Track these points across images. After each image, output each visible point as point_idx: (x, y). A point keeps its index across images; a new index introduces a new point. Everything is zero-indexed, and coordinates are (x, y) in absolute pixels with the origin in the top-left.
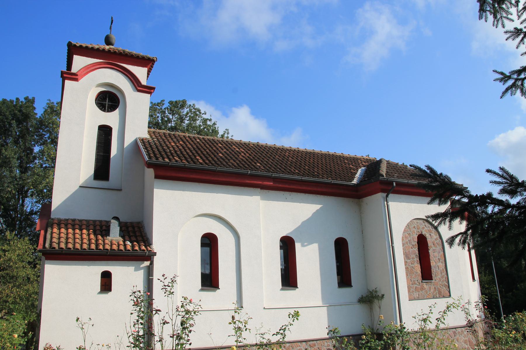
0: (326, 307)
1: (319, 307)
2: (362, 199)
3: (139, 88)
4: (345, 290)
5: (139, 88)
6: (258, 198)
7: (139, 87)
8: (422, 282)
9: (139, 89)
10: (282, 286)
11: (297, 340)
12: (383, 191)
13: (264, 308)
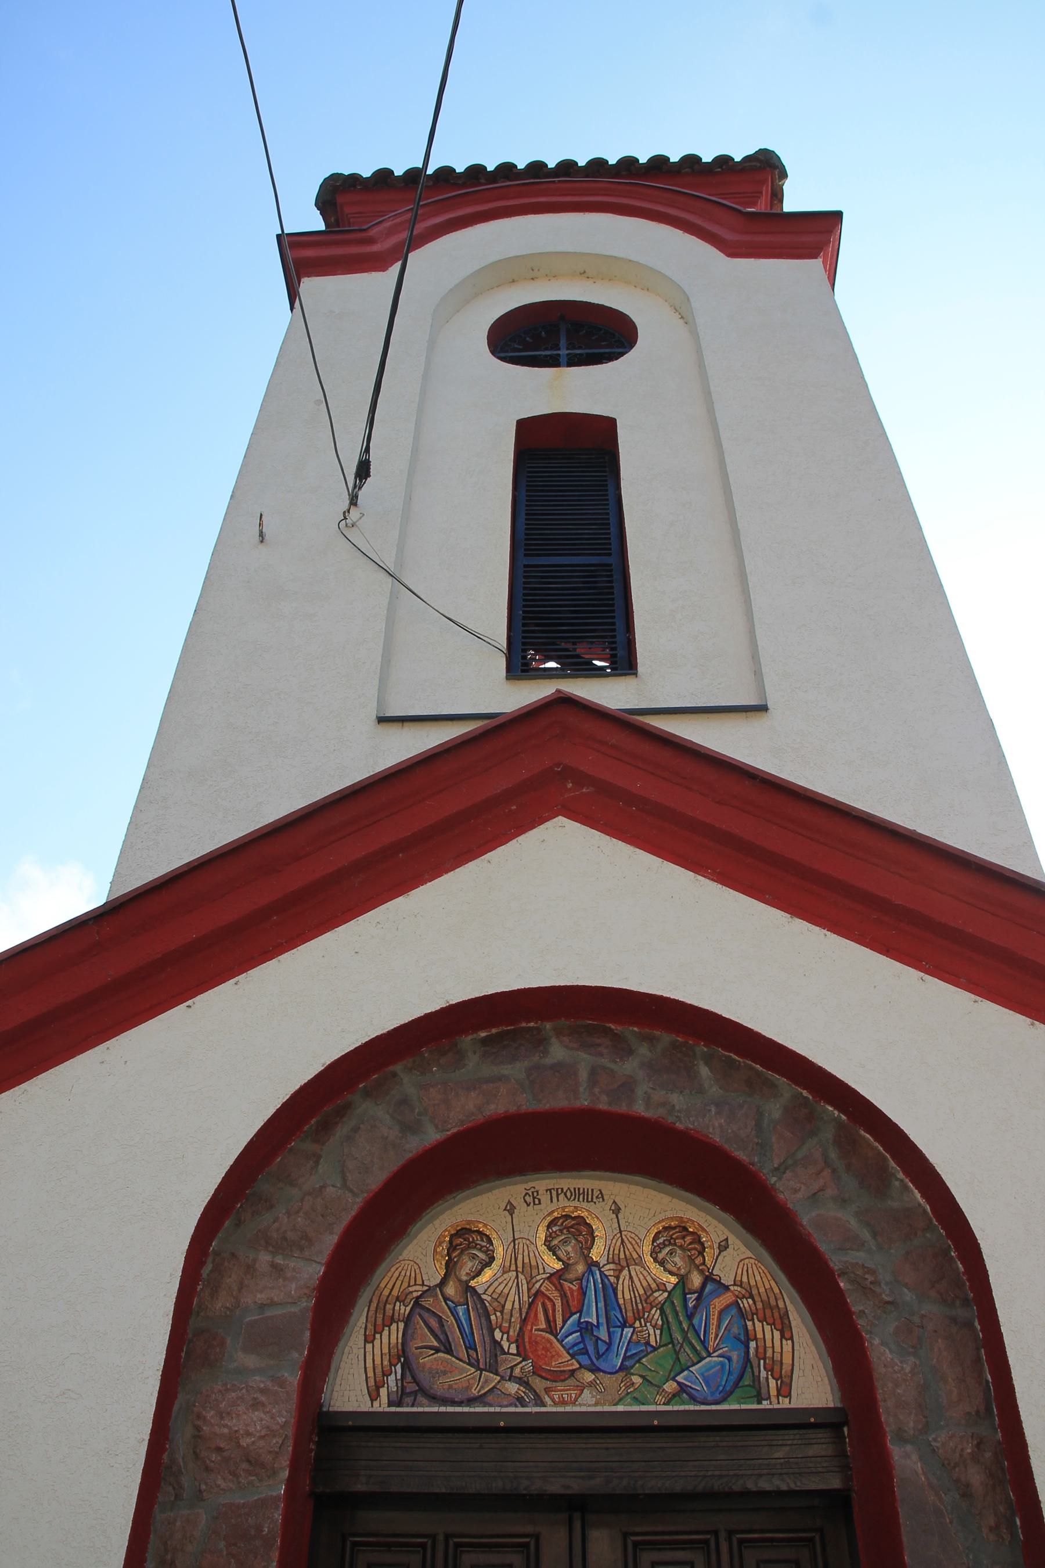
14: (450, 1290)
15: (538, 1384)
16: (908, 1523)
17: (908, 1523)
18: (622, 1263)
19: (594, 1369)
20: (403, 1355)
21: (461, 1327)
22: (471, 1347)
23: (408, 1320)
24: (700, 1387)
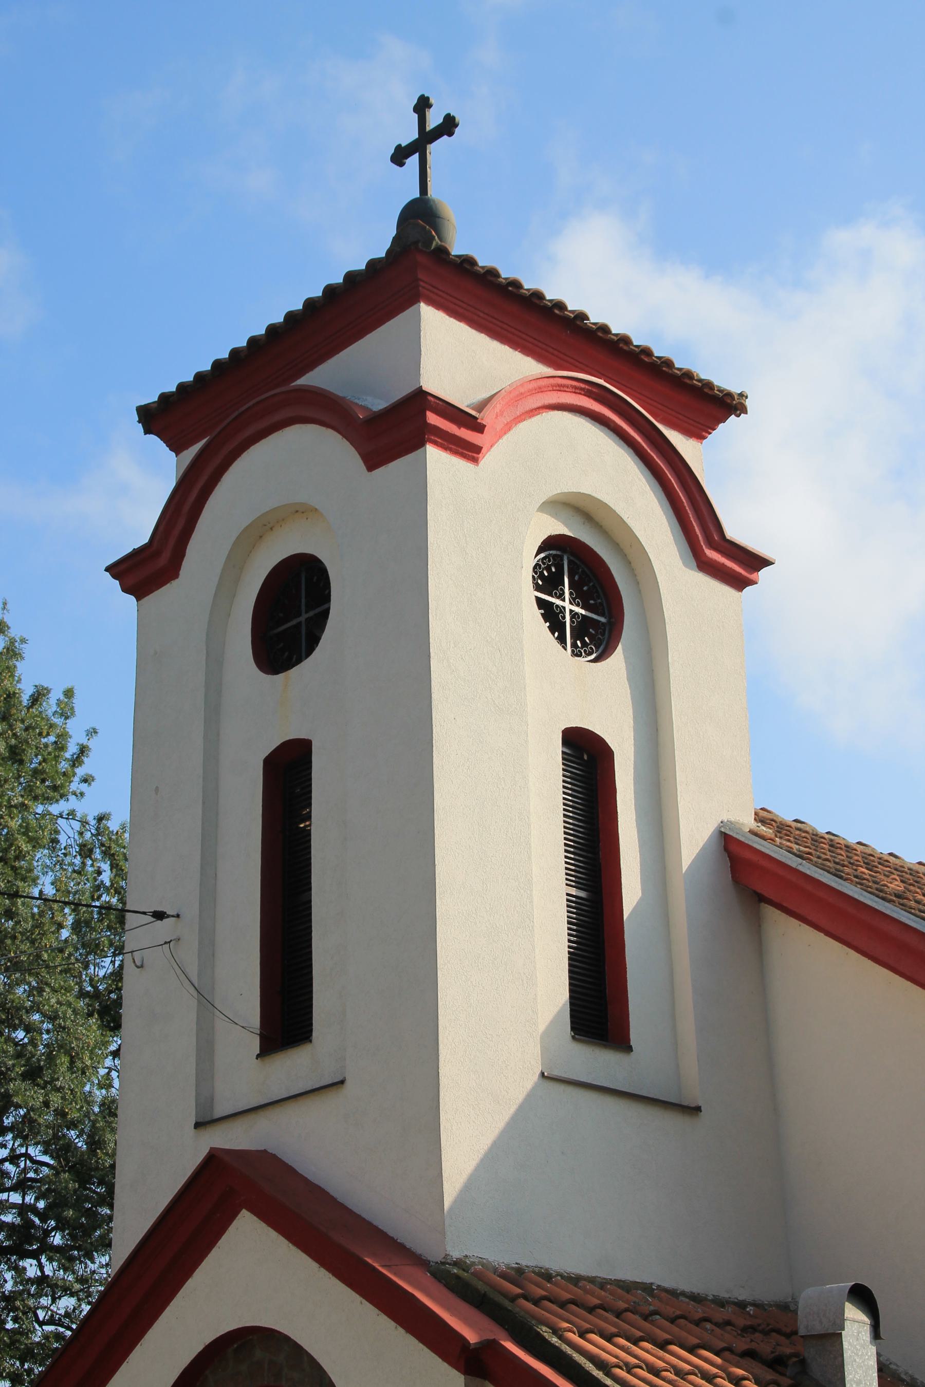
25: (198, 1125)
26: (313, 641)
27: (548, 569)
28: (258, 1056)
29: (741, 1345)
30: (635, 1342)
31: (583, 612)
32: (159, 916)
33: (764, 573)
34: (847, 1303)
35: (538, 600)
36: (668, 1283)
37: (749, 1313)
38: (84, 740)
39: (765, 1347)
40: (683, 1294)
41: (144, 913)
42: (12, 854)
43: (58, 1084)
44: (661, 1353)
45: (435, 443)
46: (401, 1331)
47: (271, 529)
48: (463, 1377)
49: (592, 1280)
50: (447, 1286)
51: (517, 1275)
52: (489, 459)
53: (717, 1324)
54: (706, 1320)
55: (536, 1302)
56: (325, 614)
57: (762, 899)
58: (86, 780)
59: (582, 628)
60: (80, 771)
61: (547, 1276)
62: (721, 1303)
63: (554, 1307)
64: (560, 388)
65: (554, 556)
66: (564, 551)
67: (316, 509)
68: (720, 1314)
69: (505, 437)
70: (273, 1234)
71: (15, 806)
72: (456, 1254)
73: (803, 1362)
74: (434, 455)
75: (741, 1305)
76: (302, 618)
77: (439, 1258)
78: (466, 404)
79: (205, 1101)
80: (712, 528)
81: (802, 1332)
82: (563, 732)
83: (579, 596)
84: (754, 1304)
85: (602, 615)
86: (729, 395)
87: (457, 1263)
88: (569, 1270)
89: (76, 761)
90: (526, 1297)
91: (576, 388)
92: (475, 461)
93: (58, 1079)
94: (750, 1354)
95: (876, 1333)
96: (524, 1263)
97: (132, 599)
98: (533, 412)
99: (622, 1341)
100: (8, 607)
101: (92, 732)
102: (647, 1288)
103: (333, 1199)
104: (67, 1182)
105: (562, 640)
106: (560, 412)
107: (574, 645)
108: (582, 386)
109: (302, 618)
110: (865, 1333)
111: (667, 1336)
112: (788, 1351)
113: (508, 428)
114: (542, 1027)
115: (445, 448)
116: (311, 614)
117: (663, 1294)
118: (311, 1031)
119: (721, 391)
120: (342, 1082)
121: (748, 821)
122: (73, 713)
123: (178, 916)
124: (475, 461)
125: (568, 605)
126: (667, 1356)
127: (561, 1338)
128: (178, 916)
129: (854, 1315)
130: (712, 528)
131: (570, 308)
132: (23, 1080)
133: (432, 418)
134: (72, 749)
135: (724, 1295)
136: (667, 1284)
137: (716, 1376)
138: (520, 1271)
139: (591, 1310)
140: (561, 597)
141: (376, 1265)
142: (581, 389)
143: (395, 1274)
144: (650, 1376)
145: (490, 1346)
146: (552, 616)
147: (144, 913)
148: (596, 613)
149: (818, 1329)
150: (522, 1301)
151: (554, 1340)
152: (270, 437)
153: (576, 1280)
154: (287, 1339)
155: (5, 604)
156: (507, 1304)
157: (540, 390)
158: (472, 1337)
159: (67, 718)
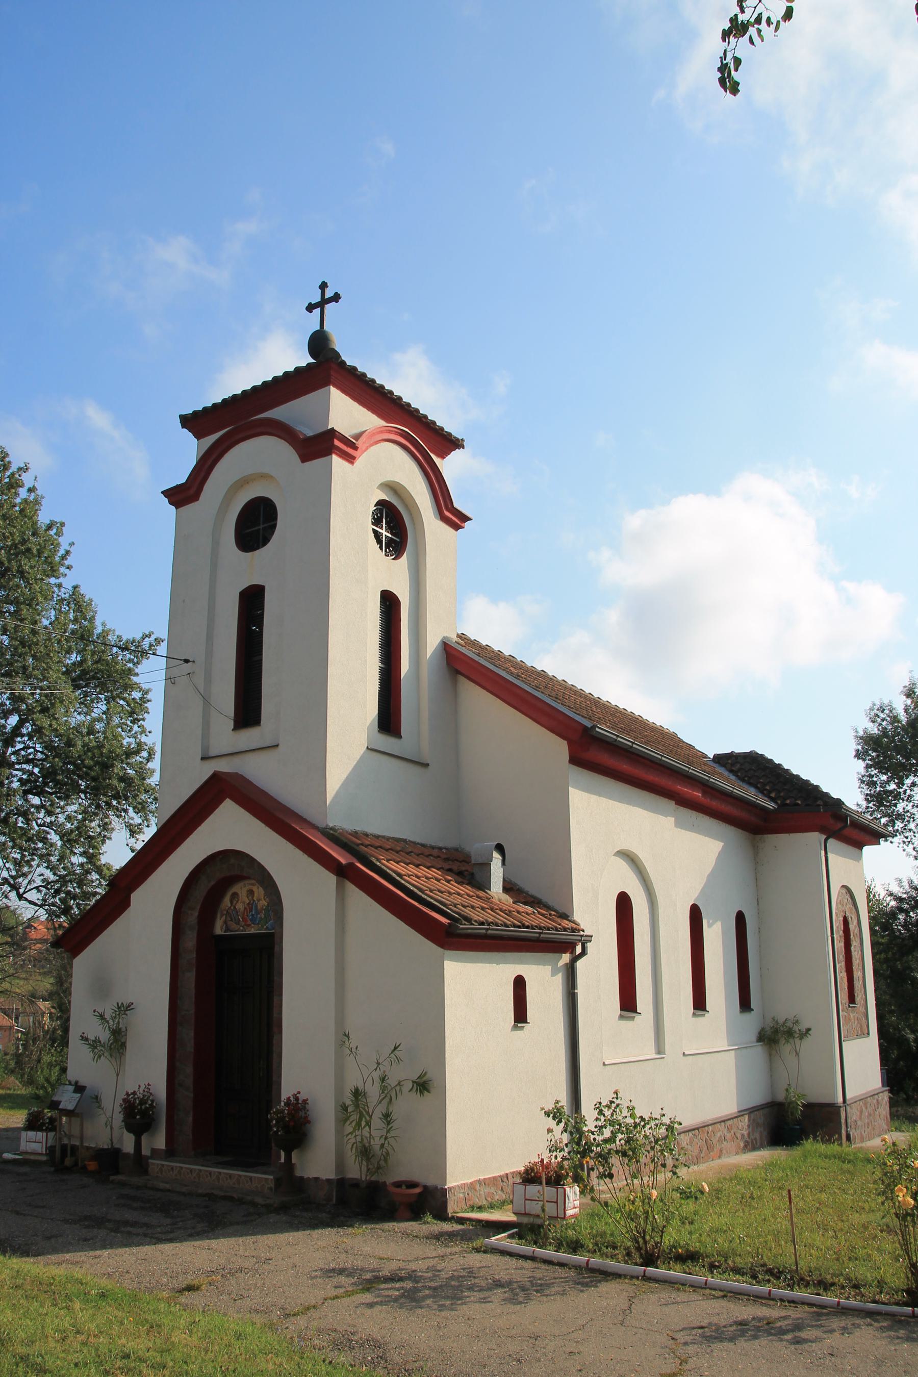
0: (734, 1051)
1: (728, 1052)
2: (760, 836)
3: (447, 514)
4: (747, 1016)
5: (447, 514)
6: (671, 820)
7: (448, 510)
8: (849, 1006)
9: (448, 517)
10: (694, 1009)
11: (728, 1115)
12: (821, 829)
13: (684, 1054)
14: (232, 908)
15: (245, 927)
16: (138, 1117)
17: (138, 1117)
18: (259, 900)
19: (254, 924)
20: (225, 922)
21: (625, 767)
22: (235, 920)
23: (226, 915)
24: (270, 927)
25: (202, 759)
26: (266, 541)
27: (377, 515)
28: (233, 730)
29: (446, 866)
30: (407, 864)
31: (390, 536)
32: (187, 661)
33: (467, 524)
34: (494, 852)
35: (373, 529)
36: (418, 840)
37: (443, 852)
38: (68, 548)
39: (455, 867)
40: (418, 843)
41: (181, 660)
42: (34, 603)
43: (56, 716)
44: (417, 869)
45: (336, 454)
46: (306, 856)
47: (248, 483)
48: (335, 877)
49: (383, 837)
50: (328, 838)
51: (355, 834)
52: (358, 463)
53: (434, 857)
54: (430, 855)
55: (366, 846)
56: (274, 526)
57: (458, 672)
58: (69, 567)
59: (390, 542)
60: (67, 563)
61: (367, 835)
62: (433, 848)
63: (373, 849)
64: (390, 432)
65: (380, 509)
66: (384, 507)
67: (272, 477)
68: (435, 853)
69: (365, 453)
70: (242, 810)
71: (38, 579)
72: (331, 825)
73: (472, 874)
74: (335, 458)
75: (440, 849)
76: (261, 527)
77: (324, 826)
78: (349, 434)
79: (205, 748)
80: (448, 501)
81: (473, 862)
82: (381, 592)
83: (390, 528)
84: (445, 848)
85: (398, 538)
86: (458, 439)
87: (331, 829)
88: (375, 833)
89: (63, 558)
90: (362, 844)
91: (396, 432)
92: (352, 463)
93: (56, 714)
94: (450, 870)
95: (504, 863)
96: (357, 829)
97: (174, 508)
98: (377, 442)
99: (402, 864)
100: (37, 479)
101: (72, 544)
102: (405, 841)
103: (272, 797)
104: (58, 763)
105: (381, 548)
106: (390, 443)
107: (386, 551)
108: (399, 431)
109: (261, 527)
110: (500, 863)
111: (419, 863)
112: (464, 869)
113: (367, 449)
114: (368, 725)
115: (340, 456)
116: (265, 525)
117: (411, 844)
118: (260, 720)
119: (455, 437)
120: (277, 746)
121: (454, 638)
122: (62, 534)
123: (194, 662)
124: (352, 463)
125: (384, 533)
126: (431, 872)
127: (380, 862)
128: (194, 662)
129: (496, 856)
130: (448, 501)
131: (395, 394)
132: (40, 714)
133: (337, 443)
134: (61, 552)
135: (433, 844)
136: (412, 840)
137: (441, 879)
138: (356, 832)
139: (387, 850)
140: (381, 528)
141: (297, 828)
142: (398, 433)
143: (306, 832)
144: (417, 879)
145: (351, 865)
146: (377, 536)
147: (181, 660)
148: (396, 537)
149: (480, 861)
150: (361, 846)
151: (378, 863)
152: (251, 440)
153: (377, 837)
154: (247, 855)
155: (36, 478)
156: (355, 847)
157: (381, 432)
158: (343, 861)
159: (59, 537)
